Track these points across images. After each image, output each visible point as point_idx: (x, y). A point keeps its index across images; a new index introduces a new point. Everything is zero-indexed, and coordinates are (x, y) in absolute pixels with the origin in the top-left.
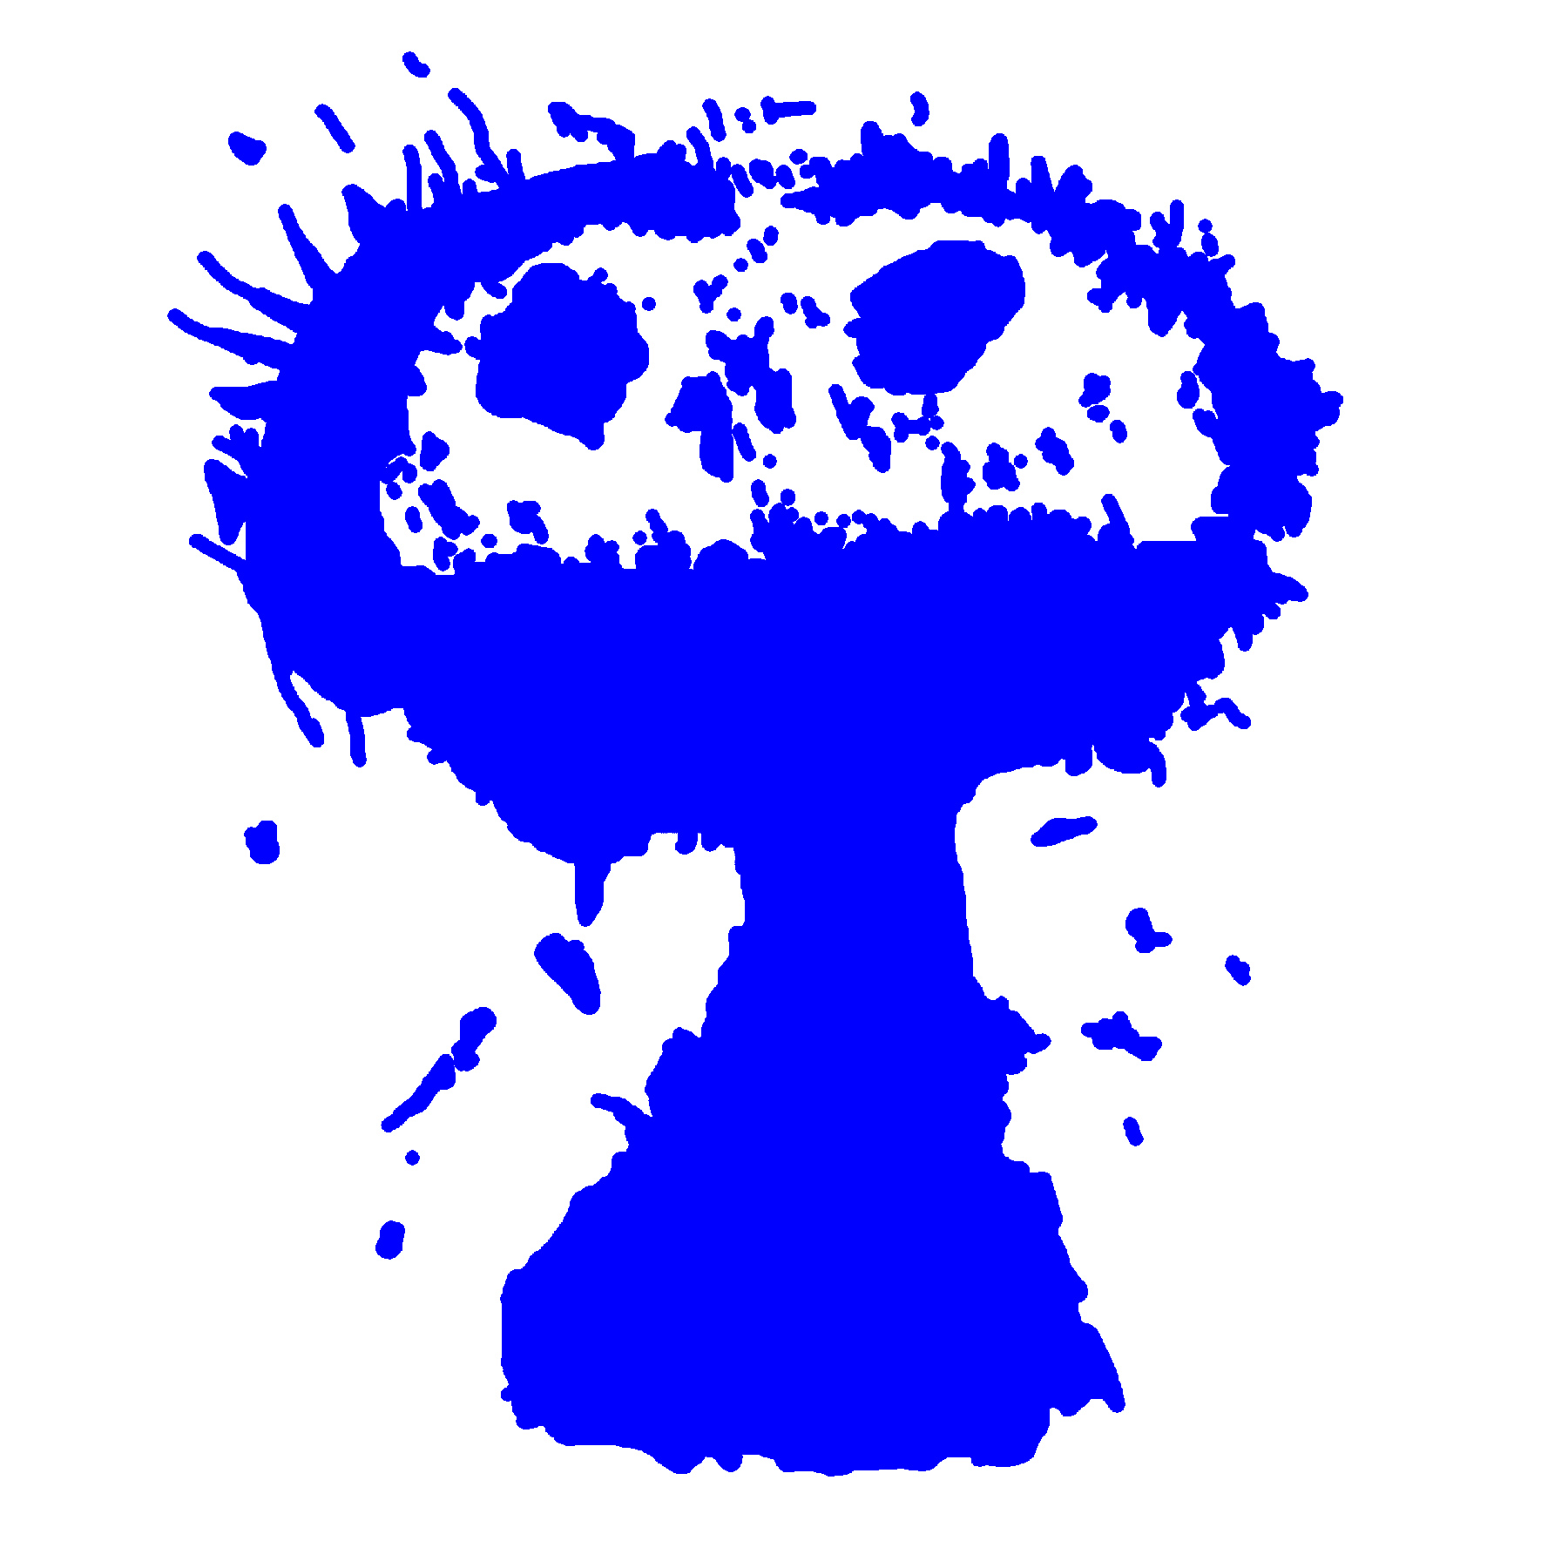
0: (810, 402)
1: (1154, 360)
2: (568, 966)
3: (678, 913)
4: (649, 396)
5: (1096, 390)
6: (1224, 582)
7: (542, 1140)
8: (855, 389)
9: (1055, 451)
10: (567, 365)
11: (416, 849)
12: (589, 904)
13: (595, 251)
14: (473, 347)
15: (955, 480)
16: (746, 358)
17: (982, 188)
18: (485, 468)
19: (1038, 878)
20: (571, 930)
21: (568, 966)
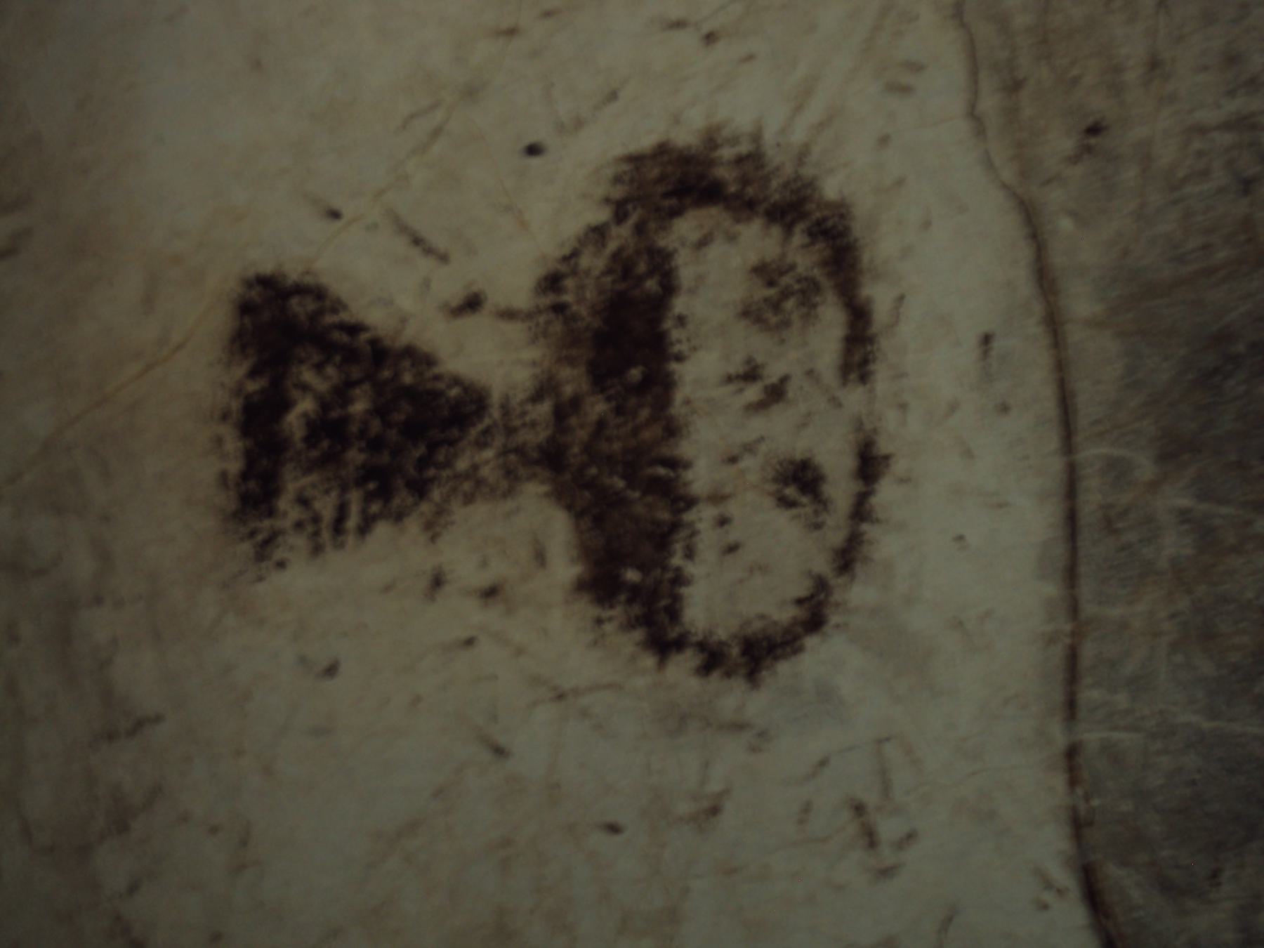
0: (757, 425)
1: (772, 604)
2: (472, 304)
3: (497, 360)
4: (756, 344)
5: (760, 568)
6: (663, 637)
7: (383, 289)
8: (763, 448)
9: (732, 549)
10: (774, 301)
11: (546, 216)
12: (509, 314)
13: (831, 320)
14: (783, 256)
15: (717, 498)
16: (776, 393)
17: (861, 511)
18: (716, 265)
19: (522, 536)
20: (488, 306)
21: (472, 304)
